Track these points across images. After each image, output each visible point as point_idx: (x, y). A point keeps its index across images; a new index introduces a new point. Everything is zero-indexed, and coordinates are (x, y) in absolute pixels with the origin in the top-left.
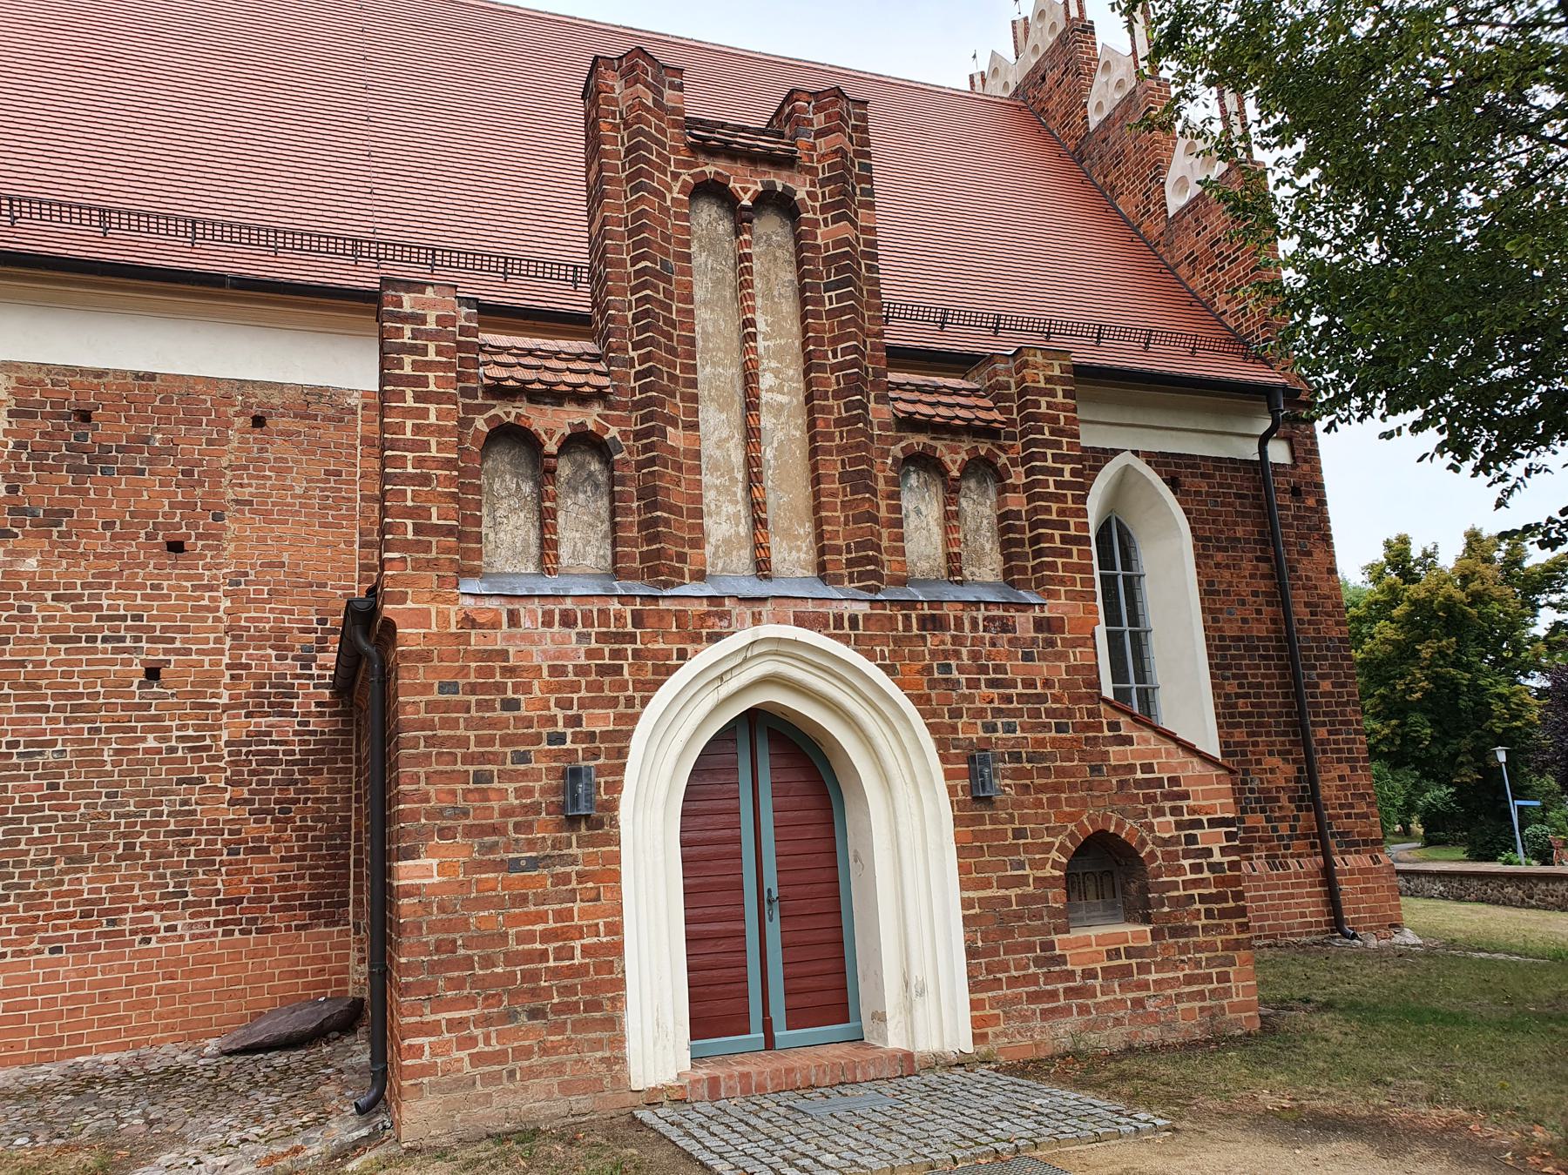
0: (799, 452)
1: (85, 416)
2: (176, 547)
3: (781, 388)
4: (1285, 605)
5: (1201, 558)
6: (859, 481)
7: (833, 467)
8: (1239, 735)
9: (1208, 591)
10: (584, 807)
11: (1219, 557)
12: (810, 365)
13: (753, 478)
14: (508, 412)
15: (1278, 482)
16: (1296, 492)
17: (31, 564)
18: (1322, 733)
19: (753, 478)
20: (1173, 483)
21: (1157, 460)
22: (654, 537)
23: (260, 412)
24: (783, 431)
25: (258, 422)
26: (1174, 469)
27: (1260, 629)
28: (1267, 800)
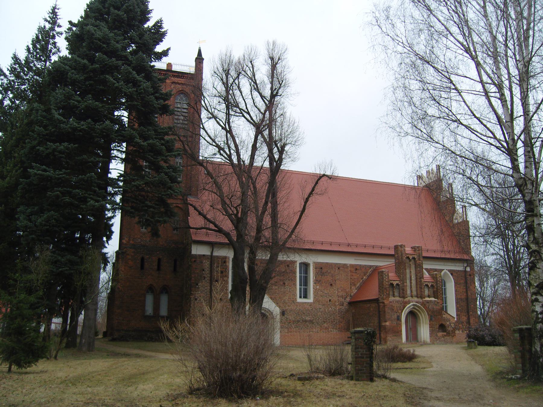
0: (415, 284)
1: (321, 268)
3: (413, 278)
4: (467, 293)
6: (421, 288)
7: (418, 286)
8: (459, 313)
9: (456, 291)
10: (399, 319)
12: (416, 276)
13: (411, 288)
14: (392, 282)
16: (470, 275)
17: (318, 287)
18: (471, 313)
19: (411, 288)
20: (452, 274)
21: (450, 271)
22: (403, 295)
23: (339, 267)
24: (414, 282)
26: (452, 272)
28: (462, 323)
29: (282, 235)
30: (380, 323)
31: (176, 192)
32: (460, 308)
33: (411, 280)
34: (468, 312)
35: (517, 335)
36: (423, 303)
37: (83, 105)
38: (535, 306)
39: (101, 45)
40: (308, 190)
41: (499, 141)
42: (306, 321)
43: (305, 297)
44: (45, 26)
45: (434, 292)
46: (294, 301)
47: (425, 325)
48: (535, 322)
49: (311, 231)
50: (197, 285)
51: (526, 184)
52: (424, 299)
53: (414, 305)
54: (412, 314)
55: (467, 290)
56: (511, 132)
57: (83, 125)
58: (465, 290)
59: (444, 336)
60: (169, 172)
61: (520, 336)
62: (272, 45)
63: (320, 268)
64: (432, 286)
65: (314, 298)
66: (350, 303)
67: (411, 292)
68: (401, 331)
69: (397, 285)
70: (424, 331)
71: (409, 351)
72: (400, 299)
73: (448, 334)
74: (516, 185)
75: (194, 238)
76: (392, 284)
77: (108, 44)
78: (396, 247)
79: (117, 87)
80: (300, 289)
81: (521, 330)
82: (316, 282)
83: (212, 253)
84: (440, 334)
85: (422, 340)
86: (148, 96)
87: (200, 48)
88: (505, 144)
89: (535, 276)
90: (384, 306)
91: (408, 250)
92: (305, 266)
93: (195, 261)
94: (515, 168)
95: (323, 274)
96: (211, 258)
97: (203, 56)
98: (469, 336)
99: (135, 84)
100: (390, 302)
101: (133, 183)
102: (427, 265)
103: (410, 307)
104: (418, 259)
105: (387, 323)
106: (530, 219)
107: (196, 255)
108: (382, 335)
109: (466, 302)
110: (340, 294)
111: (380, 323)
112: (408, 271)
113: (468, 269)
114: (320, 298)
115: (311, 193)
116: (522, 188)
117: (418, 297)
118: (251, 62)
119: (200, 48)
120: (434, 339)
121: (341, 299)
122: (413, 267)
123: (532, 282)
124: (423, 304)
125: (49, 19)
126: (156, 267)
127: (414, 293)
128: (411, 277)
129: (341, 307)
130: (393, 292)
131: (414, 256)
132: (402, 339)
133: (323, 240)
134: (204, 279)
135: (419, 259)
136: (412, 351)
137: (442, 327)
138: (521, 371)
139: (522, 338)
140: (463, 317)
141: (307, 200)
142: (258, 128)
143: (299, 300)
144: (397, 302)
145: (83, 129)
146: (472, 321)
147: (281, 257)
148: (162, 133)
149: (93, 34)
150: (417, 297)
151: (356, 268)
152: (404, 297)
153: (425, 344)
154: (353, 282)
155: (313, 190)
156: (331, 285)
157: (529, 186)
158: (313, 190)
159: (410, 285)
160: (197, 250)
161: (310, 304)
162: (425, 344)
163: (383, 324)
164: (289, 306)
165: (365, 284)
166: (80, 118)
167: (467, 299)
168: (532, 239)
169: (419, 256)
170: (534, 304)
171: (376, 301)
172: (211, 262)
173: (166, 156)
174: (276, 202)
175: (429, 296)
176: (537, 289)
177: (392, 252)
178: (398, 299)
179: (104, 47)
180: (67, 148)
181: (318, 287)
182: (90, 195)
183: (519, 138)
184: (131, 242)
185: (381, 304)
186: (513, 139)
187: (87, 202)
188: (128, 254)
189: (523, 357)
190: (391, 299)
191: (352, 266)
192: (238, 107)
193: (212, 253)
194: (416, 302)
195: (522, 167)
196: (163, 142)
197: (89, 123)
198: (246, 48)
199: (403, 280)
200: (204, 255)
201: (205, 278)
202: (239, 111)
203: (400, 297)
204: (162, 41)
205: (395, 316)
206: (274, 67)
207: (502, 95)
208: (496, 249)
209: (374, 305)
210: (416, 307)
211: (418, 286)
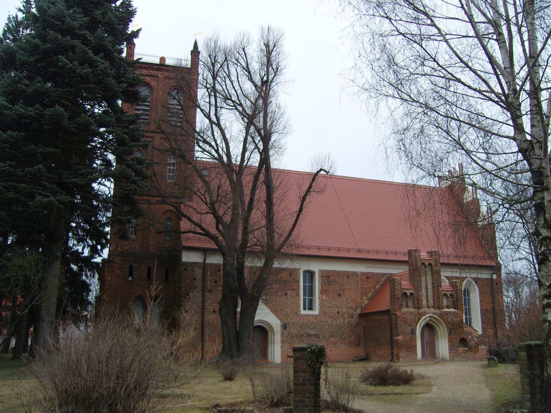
1: (328, 277)
2: (339, 295)
3: (430, 286)
5: (480, 296)
6: (439, 298)
7: (436, 296)
8: (485, 325)
9: (481, 301)
10: (413, 332)
11: (483, 295)
12: (433, 284)
13: (427, 297)
14: (405, 291)
15: (495, 282)
16: (497, 284)
17: (324, 297)
19: (427, 297)
20: (476, 283)
23: (348, 275)
24: (430, 291)
25: (348, 277)
26: (476, 280)
27: (489, 308)
28: (488, 336)
29: (278, 240)
30: (392, 336)
31: (141, 187)
32: (486, 320)
33: (427, 289)
34: (495, 325)
35: (523, 354)
36: (441, 314)
37: (30, 90)
38: (547, 313)
39: (54, 23)
40: (305, 188)
41: (497, 95)
42: (311, 335)
43: (311, 308)
44: (17, 16)
45: (454, 302)
46: (297, 313)
47: (443, 339)
48: (547, 336)
49: (309, 235)
50: (188, 295)
51: (533, 148)
52: (443, 310)
53: (430, 317)
54: (429, 327)
55: (493, 300)
56: (511, 82)
57: (30, 111)
58: (491, 300)
59: (465, 352)
60: (132, 164)
61: (527, 355)
62: (267, 31)
63: (327, 276)
64: (451, 295)
65: (320, 309)
66: (361, 316)
67: (428, 302)
68: (416, 346)
69: (411, 294)
70: (443, 347)
71: (406, 371)
72: (415, 310)
73: (471, 349)
74: (520, 151)
75: (185, 244)
76: (405, 294)
77: (63, 22)
78: (410, 252)
79: (70, 68)
80: (304, 300)
81: (528, 348)
82: (322, 291)
83: (205, 260)
84: (461, 349)
85: (441, 356)
86: (107, 78)
87: (196, 40)
88: (503, 98)
89: (547, 273)
90: (396, 318)
91: (424, 255)
92: (310, 274)
93: (185, 269)
94: (518, 128)
95: (330, 283)
96: (204, 267)
97: (199, 50)
98: (490, 352)
99: (92, 64)
100: (403, 314)
101: (89, 176)
102: (445, 273)
103: (426, 319)
104: (434, 266)
105: (400, 338)
106: (539, 195)
107: (186, 262)
108: (395, 351)
109: (493, 313)
110: (350, 305)
111: (392, 336)
112: (423, 279)
113: (495, 277)
114: (327, 310)
115: (308, 191)
116: (528, 153)
117: (435, 309)
118: (244, 49)
119: (196, 40)
120: (454, 355)
121: (351, 311)
122: (429, 274)
123: (543, 281)
124: (441, 315)
125: (22, 8)
126: (146, 276)
127: (431, 303)
128: (427, 285)
129: (350, 319)
130: (407, 302)
131: (430, 262)
132: (416, 355)
133: (330, 246)
134: (196, 289)
135: (436, 266)
136: (409, 372)
137: (464, 342)
138: (529, 404)
139: (530, 358)
140: (489, 330)
141: (304, 199)
142: (250, 120)
143: (303, 312)
144: (411, 313)
145: (30, 115)
146: (499, 335)
147: (276, 265)
148: (128, 121)
149: (46, 11)
150: (434, 307)
151: (368, 276)
152: (419, 308)
153: (444, 360)
154: (364, 291)
155: (310, 187)
156: (339, 295)
157: (537, 151)
158: (310, 187)
159: (426, 293)
160: (187, 257)
161: (315, 316)
162: (444, 360)
163: (396, 338)
164: (291, 318)
165: (377, 293)
166: (29, 102)
167: (494, 310)
168: (543, 222)
169: (436, 262)
170: (546, 310)
171: (388, 312)
172: (204, 270)
173: (129, 147)
174: (272, 203)
175: (448, 307)
176: (549, 290)
177: (406, 258)
178: (412, 310)
179: (57, 25)
180: (13, 137)
181: (324, 297)
182: (39, 190)
183: (521, 88)
184: (119, 249)
185: (393, 316)
186: (515, 90)
187: (35, 197)
188: (115, 263)
189: (531, 384)
190: (405, 310)
191: (363, 274)
192: (231, 100)
193: (205, 260)
194: (433, 314)
195: (527, 128)
196: (126, 130)
197: (38, 109)
198: (238, 34)
199: (418, 288)
200: (196, 263)
201: (196, 287)
202: (232, 104)
203: (414, 308)
204: (131, 21)
205: (408, 330)
206: (269, 53)
207: (500, 34)
208: (524, 253)
209: (385, 317)
210: (433, 319)
211: (436, 296)
